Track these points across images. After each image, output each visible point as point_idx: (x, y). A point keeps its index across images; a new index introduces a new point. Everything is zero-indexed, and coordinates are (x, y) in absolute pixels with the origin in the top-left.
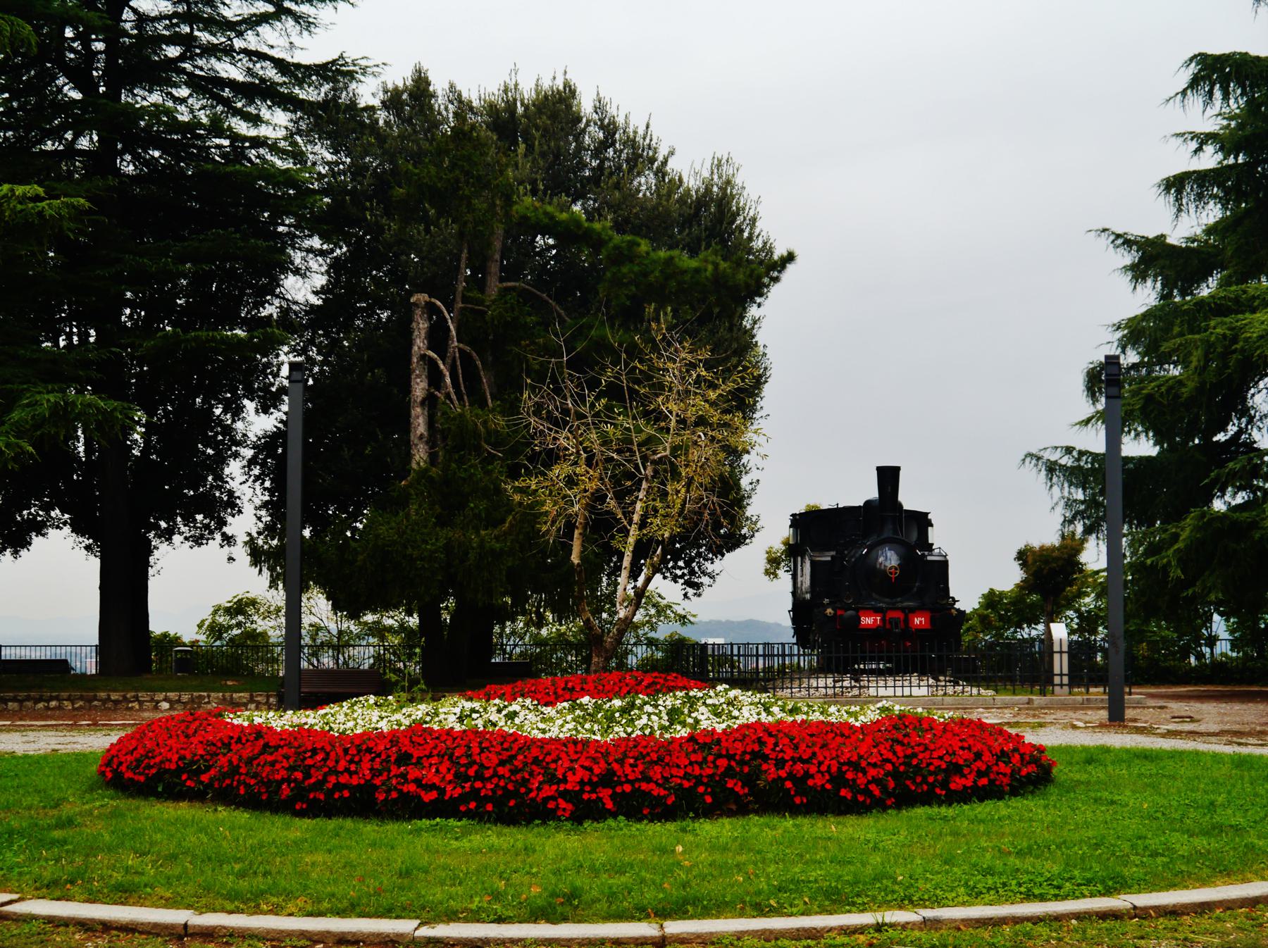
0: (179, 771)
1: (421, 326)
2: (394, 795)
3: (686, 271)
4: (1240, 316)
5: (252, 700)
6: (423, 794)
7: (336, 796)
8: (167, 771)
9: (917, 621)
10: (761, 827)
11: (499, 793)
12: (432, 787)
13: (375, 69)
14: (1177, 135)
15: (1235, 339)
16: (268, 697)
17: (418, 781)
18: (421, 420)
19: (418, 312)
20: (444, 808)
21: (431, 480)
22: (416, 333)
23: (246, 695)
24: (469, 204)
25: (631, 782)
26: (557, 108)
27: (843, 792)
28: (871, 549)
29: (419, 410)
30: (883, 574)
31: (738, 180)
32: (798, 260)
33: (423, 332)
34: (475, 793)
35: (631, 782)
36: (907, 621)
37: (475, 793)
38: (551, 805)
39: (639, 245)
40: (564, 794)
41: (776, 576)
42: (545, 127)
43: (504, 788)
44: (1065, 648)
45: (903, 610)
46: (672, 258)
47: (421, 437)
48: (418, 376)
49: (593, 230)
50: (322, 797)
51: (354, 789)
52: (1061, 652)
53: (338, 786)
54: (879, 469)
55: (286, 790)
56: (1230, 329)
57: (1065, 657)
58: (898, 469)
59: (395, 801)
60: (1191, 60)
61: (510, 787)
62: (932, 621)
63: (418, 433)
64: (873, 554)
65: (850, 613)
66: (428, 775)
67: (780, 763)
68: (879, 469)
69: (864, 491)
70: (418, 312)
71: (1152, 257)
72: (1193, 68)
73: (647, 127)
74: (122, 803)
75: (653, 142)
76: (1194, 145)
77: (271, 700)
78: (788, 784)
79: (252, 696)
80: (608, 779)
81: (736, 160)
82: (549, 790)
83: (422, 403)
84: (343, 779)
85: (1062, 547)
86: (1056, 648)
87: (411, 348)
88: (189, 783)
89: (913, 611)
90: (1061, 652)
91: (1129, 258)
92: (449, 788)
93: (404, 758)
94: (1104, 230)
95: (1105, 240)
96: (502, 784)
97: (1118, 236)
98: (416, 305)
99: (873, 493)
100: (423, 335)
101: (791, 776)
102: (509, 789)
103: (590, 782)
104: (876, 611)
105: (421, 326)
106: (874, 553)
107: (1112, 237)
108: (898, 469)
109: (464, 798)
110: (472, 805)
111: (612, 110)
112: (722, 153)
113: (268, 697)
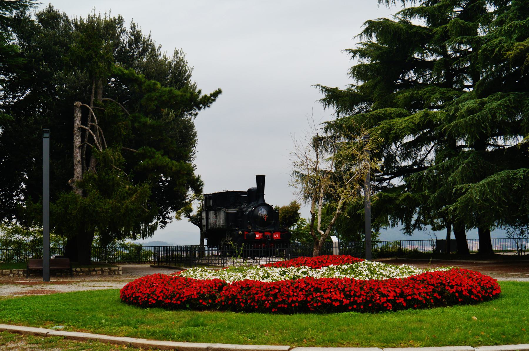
0: (199, 299)
1: (78, 115)
2: (320, 304)
3: (178, 96)
4: (392, 120)
5: (11, 273)
6: (334, 303)
7: (293, 305)
8: (192, 299)
9: (275, 236)
10: (465, 311)
11: (364, 301)
12: (336, 300)
13: (36, 5)
14: (346, 50)
15: (391, 129)
16: (18, 271)
17: (330, 298)
18: (79, 155)
19: (77, 109)
20: (342, 308)
21: (94, 179)
22: (76, 118)
23: (9, 271)
24: (97, 65)
25: (410, 295)
26: (112, 27)
27: (472, 297)
28: (256, 207)
29: (78, 150)
30: (262, 218)
31: (185, 59)
32: (223, 93)
33: (79, 118)
34: (355, 302)
35: (410, 295)
36: (272, 236)
37: (355, 302)
38: (385, 305)
39: (157, 84)
40: (388, 301)
41: (180, 219)
42: (100, 33)
43: (366, 299)
44: (337, 245)
45: (270, 232)
46: (171, 90)
47: (79, 162)
48: (77, 136)
49: (139, 77)
50: (286, 306)
51: (301, 302)
52: (336, 247)
53: (293, 302)
54: (257, 176)
55: (268, 304)
56: (389, 125)
57: (337, 248)
58: (264, 176)
59: (319, 307)
60: (366, 22)
61: (368, 299)
62: (281, 236)
63: (78, 160)
64: (256, 210)
65: (252, 233)
66: (334, 296)
67: (452, 287)
68: (257, 176)
69: (245, 184)
70: (77, 109)
71: (333, 96)
72: (367, 26)
73: (149, 36)
74: (139, 312)
75: (153, 42)
76: (352, 54)
77: (20, 272)
78: (457, 295)
79: (11, 271)
80: (402, 295)
81: (184, 51)
82: (384, 299)
83: (79, 147)
84: (295, 299)
85: (291, 208)
86: (334, 246)
87: (73, 125)
88: (204, 303)
89: (275, 232)
90: (336, 247)
91: (323, 95)
92: (345, 300)
93: (317, 290)
94: (318, 85)
95: (319, 89)
96: (364, 298)
97: (324, 88)
98: (76, 106)
99: (254, 185)
100: (79, 119)
101: (457, 291)
102: (371, 300)
103: (397, 296)
104: (260, 232)
105: (78, 115)
106: (257, 209)
107: (321, 88)
108: (264, 176)
109: (352, 304)
110: (355, 307)
111: (138, 29)
112: (178, 48)
113: (18, 271)
